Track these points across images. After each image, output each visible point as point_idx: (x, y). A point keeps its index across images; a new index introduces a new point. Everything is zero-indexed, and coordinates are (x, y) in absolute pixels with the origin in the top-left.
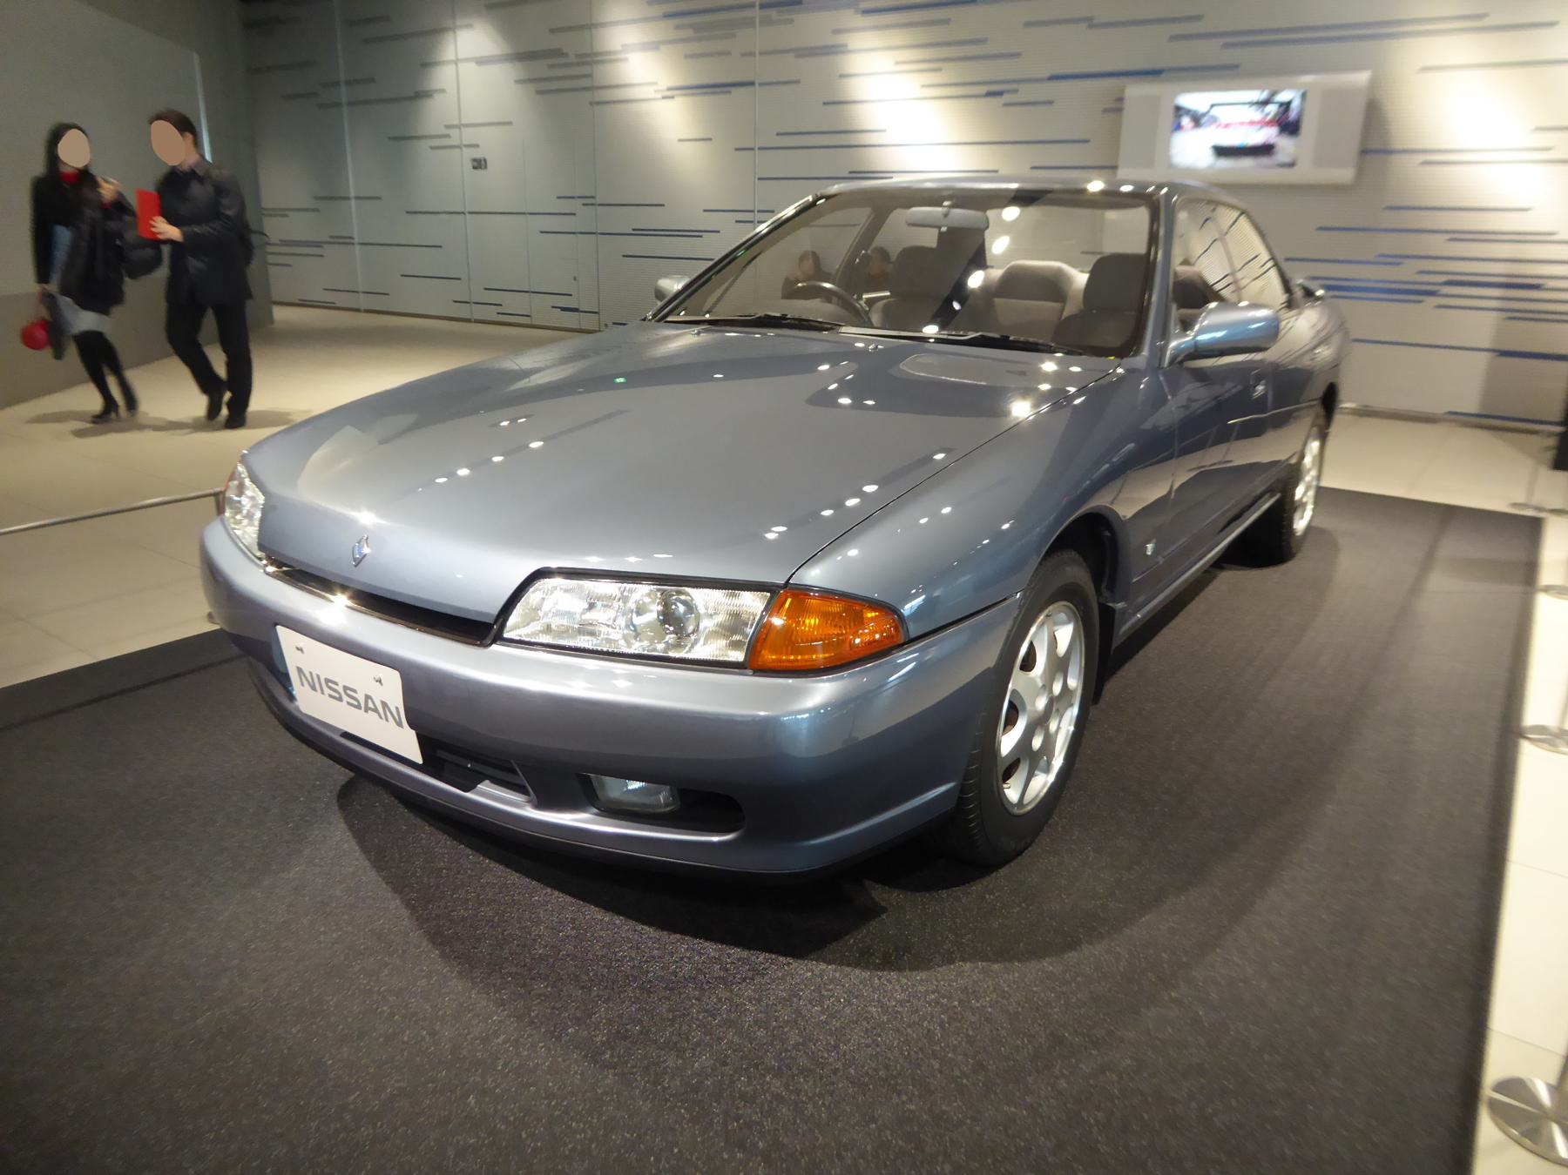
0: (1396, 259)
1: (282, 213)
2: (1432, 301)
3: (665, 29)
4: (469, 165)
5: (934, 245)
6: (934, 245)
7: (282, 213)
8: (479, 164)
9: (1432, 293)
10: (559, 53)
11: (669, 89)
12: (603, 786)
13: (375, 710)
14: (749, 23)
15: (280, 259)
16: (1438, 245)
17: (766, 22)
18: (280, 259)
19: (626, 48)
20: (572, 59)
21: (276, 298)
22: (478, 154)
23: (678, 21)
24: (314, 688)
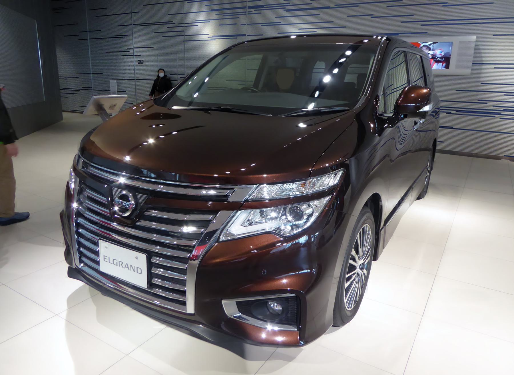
0: (485, 102)
1: (65, 78)
2: (498, 117)
3: (213, 15)
4: (136, 62)
5: (223, 302)
6: (223, 302)
7: (65, 78)
8: (140, 62)
9: (499, 114)
10: (171, 22)
11: (213, 36)
12: (73, 203)
13: (128, 267)
14: (244, 13)
15: (65, 95)
16: (501, 97)
17: (250, 13)
18: (65, 95)
19: (198, 22)
20: (176, 25)
21: (63, 109)
22: (138, 58)
23: (217, 12)
24: (134, 271)
